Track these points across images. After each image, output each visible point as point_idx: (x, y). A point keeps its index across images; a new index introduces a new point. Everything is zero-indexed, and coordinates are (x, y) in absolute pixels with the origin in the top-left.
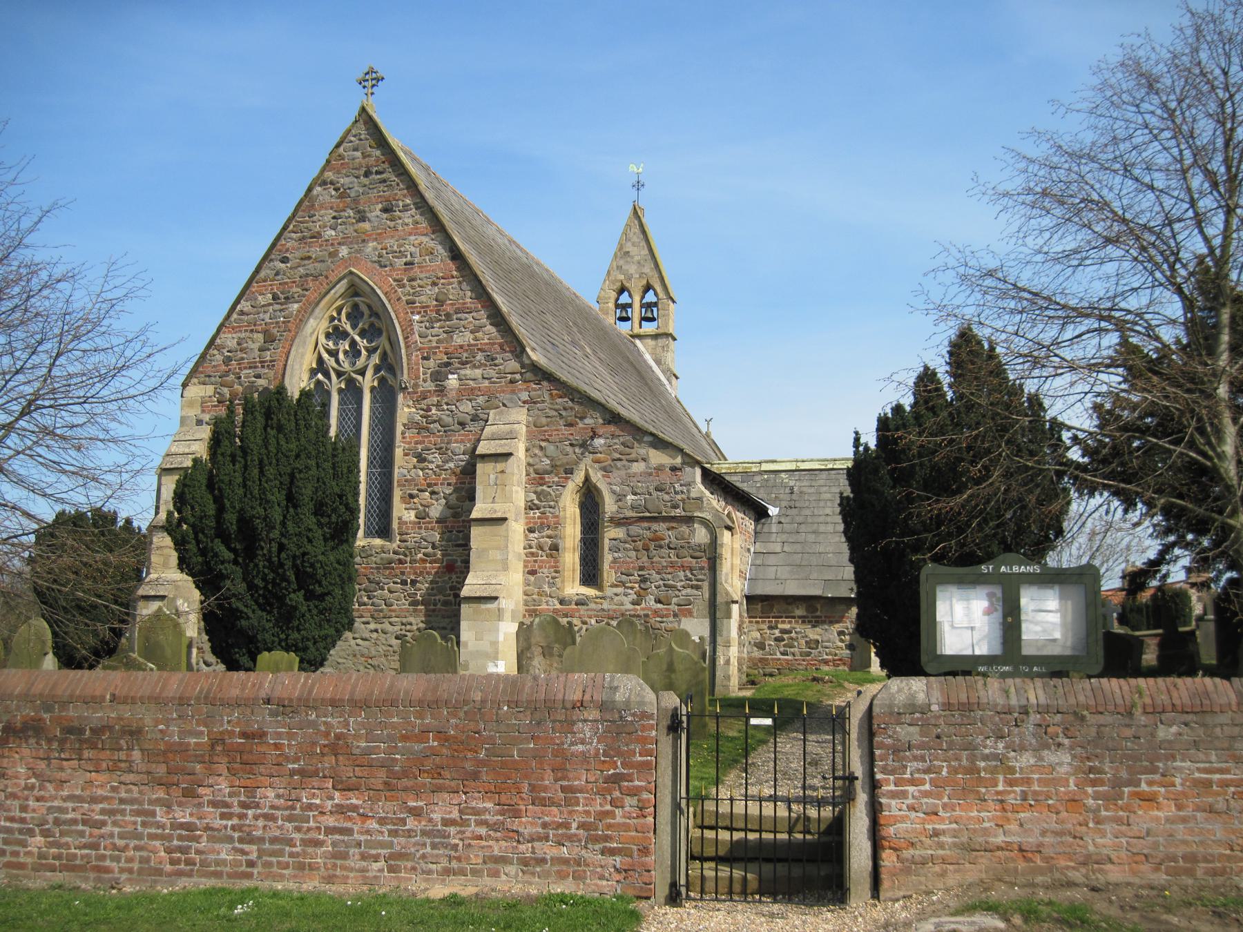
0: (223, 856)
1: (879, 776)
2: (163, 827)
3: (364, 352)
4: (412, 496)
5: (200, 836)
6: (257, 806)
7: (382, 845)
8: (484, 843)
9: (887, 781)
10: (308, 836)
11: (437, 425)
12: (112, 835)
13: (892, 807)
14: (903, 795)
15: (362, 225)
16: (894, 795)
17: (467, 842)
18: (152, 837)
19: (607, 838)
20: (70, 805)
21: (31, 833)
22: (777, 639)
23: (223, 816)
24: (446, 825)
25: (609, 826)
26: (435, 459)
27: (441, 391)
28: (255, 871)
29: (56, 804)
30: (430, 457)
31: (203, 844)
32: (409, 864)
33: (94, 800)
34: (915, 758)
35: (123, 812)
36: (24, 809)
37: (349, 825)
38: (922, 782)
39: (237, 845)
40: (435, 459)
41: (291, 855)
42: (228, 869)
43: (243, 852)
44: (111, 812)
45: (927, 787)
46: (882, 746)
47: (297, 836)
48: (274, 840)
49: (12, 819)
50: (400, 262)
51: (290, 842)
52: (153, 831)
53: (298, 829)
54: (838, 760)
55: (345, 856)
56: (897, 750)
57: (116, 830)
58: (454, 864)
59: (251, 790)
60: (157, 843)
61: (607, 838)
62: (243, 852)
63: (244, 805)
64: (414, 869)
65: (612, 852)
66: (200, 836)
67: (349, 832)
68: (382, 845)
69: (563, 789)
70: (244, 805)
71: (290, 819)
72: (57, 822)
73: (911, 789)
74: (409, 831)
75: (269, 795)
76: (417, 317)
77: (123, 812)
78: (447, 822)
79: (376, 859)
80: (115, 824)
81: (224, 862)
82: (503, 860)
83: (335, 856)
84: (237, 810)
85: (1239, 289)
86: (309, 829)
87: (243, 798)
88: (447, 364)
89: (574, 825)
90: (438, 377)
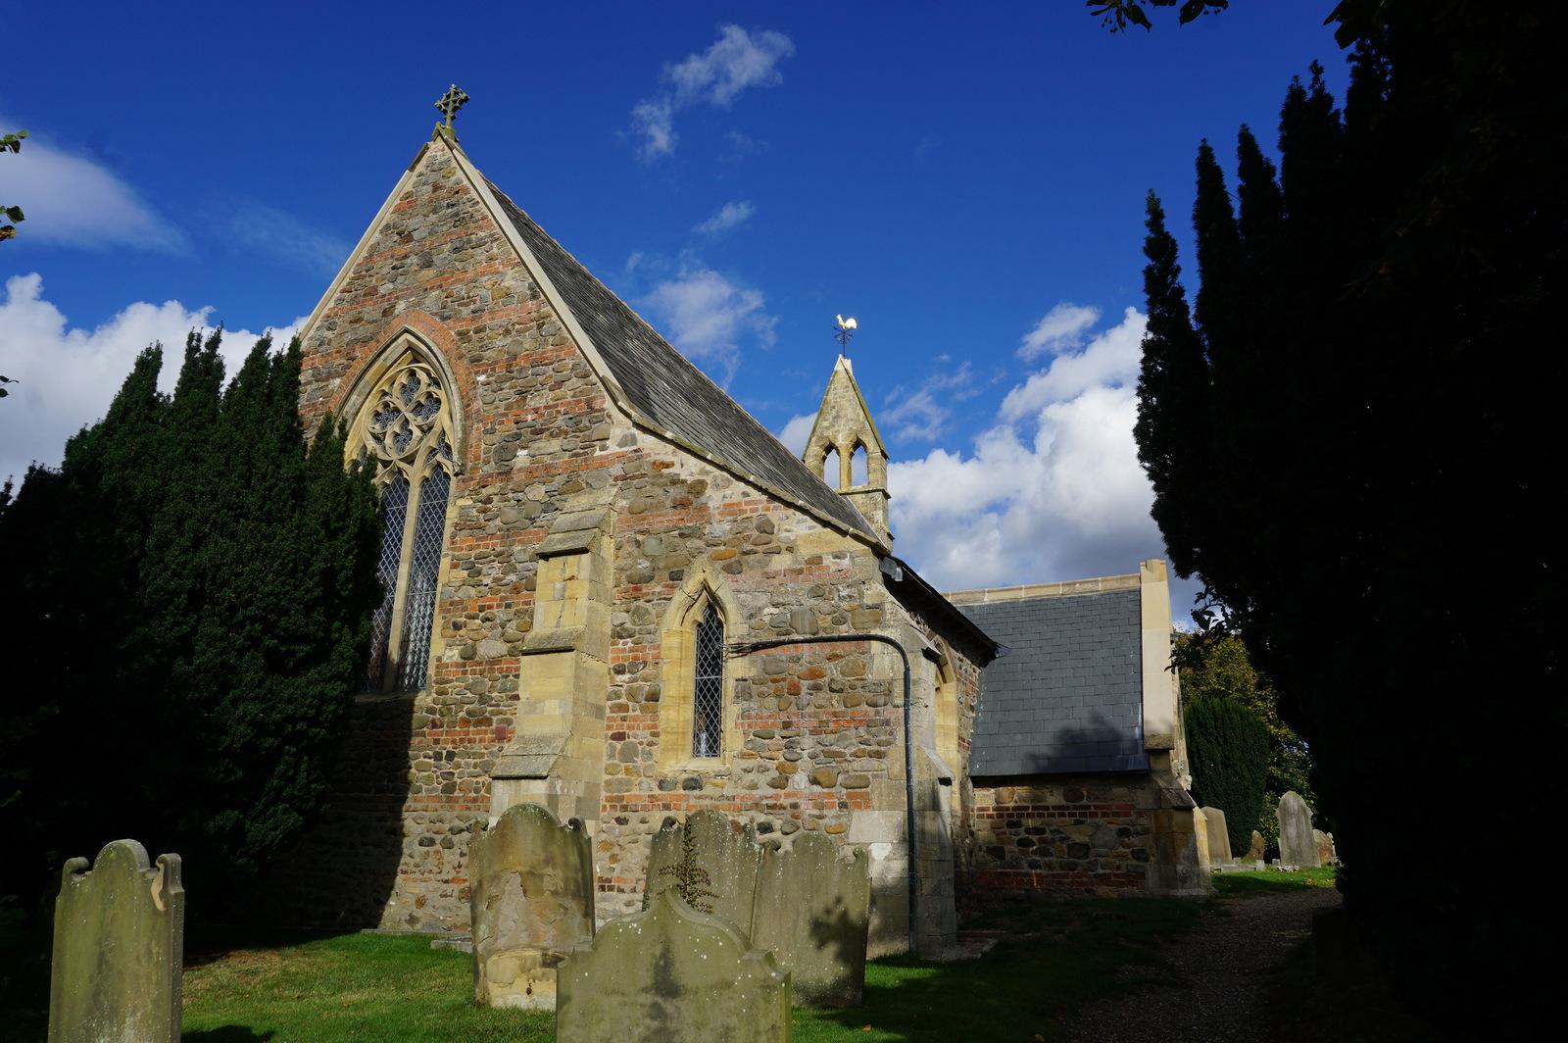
4: (457, 627)
27: (506, 474)
42: (1116, 803)
50: (466, 312)
88: (517, 436)
90: (505, 454)
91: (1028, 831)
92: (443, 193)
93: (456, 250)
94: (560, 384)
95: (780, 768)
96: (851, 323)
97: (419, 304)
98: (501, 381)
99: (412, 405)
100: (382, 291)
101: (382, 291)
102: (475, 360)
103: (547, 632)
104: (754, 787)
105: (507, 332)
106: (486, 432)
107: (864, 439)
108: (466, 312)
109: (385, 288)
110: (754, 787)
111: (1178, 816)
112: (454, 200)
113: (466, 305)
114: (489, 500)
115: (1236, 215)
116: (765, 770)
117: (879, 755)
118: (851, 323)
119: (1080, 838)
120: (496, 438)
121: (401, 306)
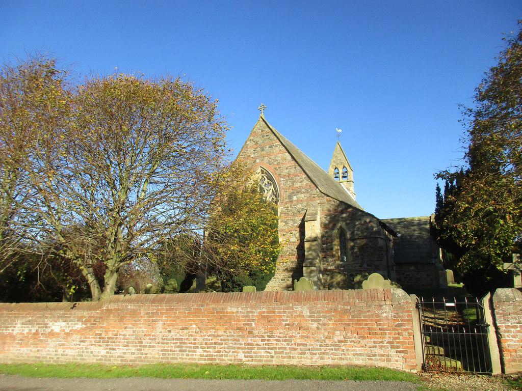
0: (263, 354)
1: (498, 325)
2: (242, 344)
3: (266, 191)
4: (284, 235)
5: (255, 348)
6: (274, 337)
7: (317, 349)
8: (353, 348)
9: (502, 326)
10: (292, 347)
11: (291, 212)
12: (225, 348)
13: (505, 336)
14: (509, 331)
15: (263, 152)
16: (505, 332)
17: (347, 348)
18: (238, 348)
19: (398, 347)
20: (210, 338)
21: (197, 347)
22: (405, 278)
23: (262, 340)
24: (339, 342)
25: (398, 343)
26: (291, 223)
27: (291, 201)
28: (274, 359)
29: (206, 338)
30: (289, 222)
31: (256, 350)
32: (327, 356)
33: (218, 336)
34: (512, 318)
35: (228, 340)
36: (195, 340)
37: (306, 343)
38: (517, 327)
39: (267, 350)
40: (291, 223)
41: (286, 353)
42: (265, 359)
43: (270, 353)
44: (224, 340)
45: (519, 329)
46: (498, 313)
47: (288, 347)
48: (280, 348)
49: (191, 343)
50: (276, 163)
51: (285, 349)
52: (238, 346)
53: (288, 344)
54: (430, 320)
55: (305, 353)
56: (504, 315)
57: (226, 346)
58: (343, 356)
59: (271, 331)
60: (240, 350)
61: (398, 347)
62: (270, 353)
63: (269, 336)
64: (329, 358)
65: (400, 352)
66: (255, 348)
67: (305, 345)
68: (317, 349)
69: (380, 329)
70: (269, 336)
71: (285, 341)
72: (206, 344)
73: (512, 329)
74: (327, 344)
75: (277, 333)
76: (282, 179)
77: (228, 340)
78: (340, 341)
79: (315, 354)
80: (226, 344)
81: (263, 357)
82: (361, 355)
83: (301, 353)
84: (267, 338)
85: (519, 149)
86: (292, 344)
87: (269, 334)
88: (293, 193)
89: (385, 342)
90: (290, 197)
91: (406, 275)
92: (264, 132)
93: (270, 147)
94: (302, 182)
95: (361, 263)
96: (340, 131)
97: (263, 160)
98: (287, 180)
99: (264, 184)
100: (252, 156)
101: (252, 156)
102: (280, 175)
103: (309, 235)
104: (355, 267)
105: (287, 168)
106: (285, 192)
107: (346, 166)
108: (276, 163)
109: (253, 156)
110: (355, 267)
111: (440, 272)
112: (267, 134)
113: (275, 161)
114: (288, 207)
115: (440, 249)
116: (358, 263)
117: (381, 261)
118: (340, 131)
119: (417, 276)
120: (288, 193)
121: (258, 161)
